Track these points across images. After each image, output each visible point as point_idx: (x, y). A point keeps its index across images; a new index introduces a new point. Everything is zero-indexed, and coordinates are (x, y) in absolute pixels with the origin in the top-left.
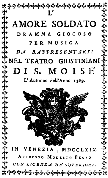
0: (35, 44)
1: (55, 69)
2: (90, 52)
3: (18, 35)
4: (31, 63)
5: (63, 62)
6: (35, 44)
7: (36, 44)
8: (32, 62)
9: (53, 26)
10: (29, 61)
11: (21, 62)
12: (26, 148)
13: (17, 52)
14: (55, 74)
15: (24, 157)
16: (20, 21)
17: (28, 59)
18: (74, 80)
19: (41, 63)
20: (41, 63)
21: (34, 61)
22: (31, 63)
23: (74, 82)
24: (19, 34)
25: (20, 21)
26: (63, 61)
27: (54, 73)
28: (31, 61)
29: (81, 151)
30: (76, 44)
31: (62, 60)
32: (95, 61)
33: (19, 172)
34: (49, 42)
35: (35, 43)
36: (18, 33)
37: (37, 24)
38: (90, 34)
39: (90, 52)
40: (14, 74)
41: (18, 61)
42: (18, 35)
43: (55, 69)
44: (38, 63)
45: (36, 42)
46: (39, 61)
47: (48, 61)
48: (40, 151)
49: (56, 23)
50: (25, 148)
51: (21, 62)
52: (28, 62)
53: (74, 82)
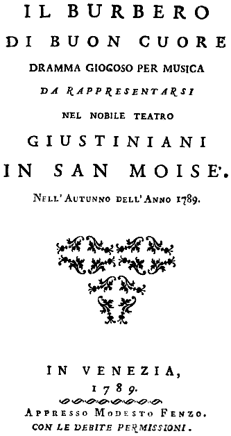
0: (156, 16)
1: (142, 166)
2: (187, 92)
3: (31, 70)
4: (142, 119)
5: (94, 70)
6: (156, 16)
7: (159, 15)
8: (131, 373)
9: (192, 176)
10: (140, 117)
11: (49, 16)
12: (86, 369)
13: (9, 42)
14: (143, 176)
15: (38, 412)
16: (131, 165)
17: (100, 137)
18: (178, 198)
19: (157, 118)
20: (157, 118)
21: (147, 116)
22: (142, 119)
23: (179, 201)
24: (44, 91)
25: (131, 165)
26: (94, 67)
27: (140, 174)
28: (142, 116)
29: (42, 16)
30: (29, 414)
31: (37, 137)
32: (114, 42)
33: (78, 401)
34: (133, 166)
35: (156, 12)
36: (8, 38)
37: (56, 41)
38: (66, 401)
39: (187, 92)
40: (101, 5)
41: (128, 200)
42: (31, 70)
43: (142, 166)
44: (152, 119)
45: (159, 9)
46: (154, 116)
47: (166, 117)
48: (225, 46)
49: (121, 69)
50: (84, 367)
51: (49, 16)
52: (137, 118)
53: (179, 201)
